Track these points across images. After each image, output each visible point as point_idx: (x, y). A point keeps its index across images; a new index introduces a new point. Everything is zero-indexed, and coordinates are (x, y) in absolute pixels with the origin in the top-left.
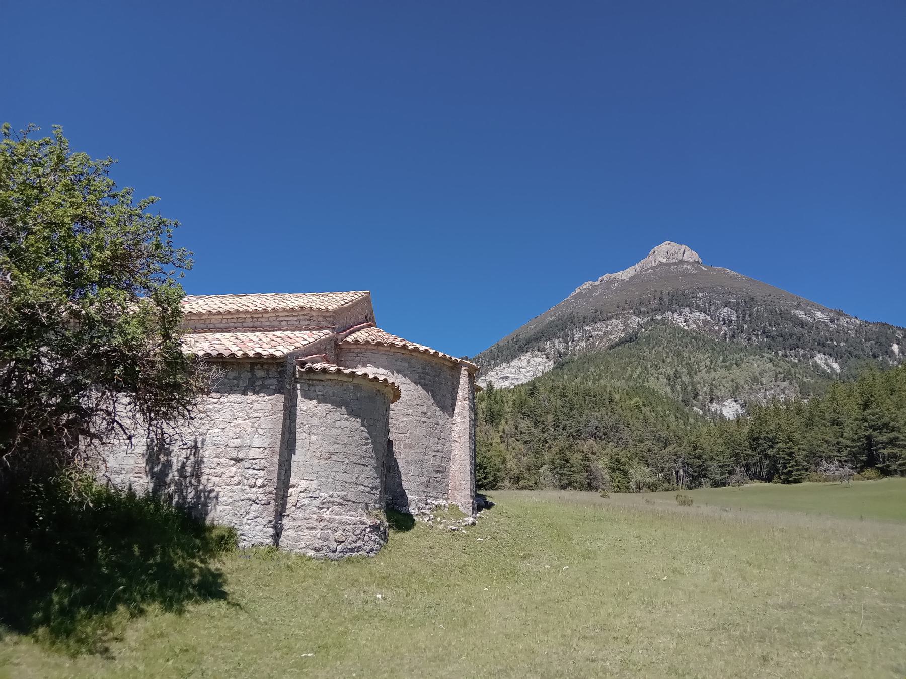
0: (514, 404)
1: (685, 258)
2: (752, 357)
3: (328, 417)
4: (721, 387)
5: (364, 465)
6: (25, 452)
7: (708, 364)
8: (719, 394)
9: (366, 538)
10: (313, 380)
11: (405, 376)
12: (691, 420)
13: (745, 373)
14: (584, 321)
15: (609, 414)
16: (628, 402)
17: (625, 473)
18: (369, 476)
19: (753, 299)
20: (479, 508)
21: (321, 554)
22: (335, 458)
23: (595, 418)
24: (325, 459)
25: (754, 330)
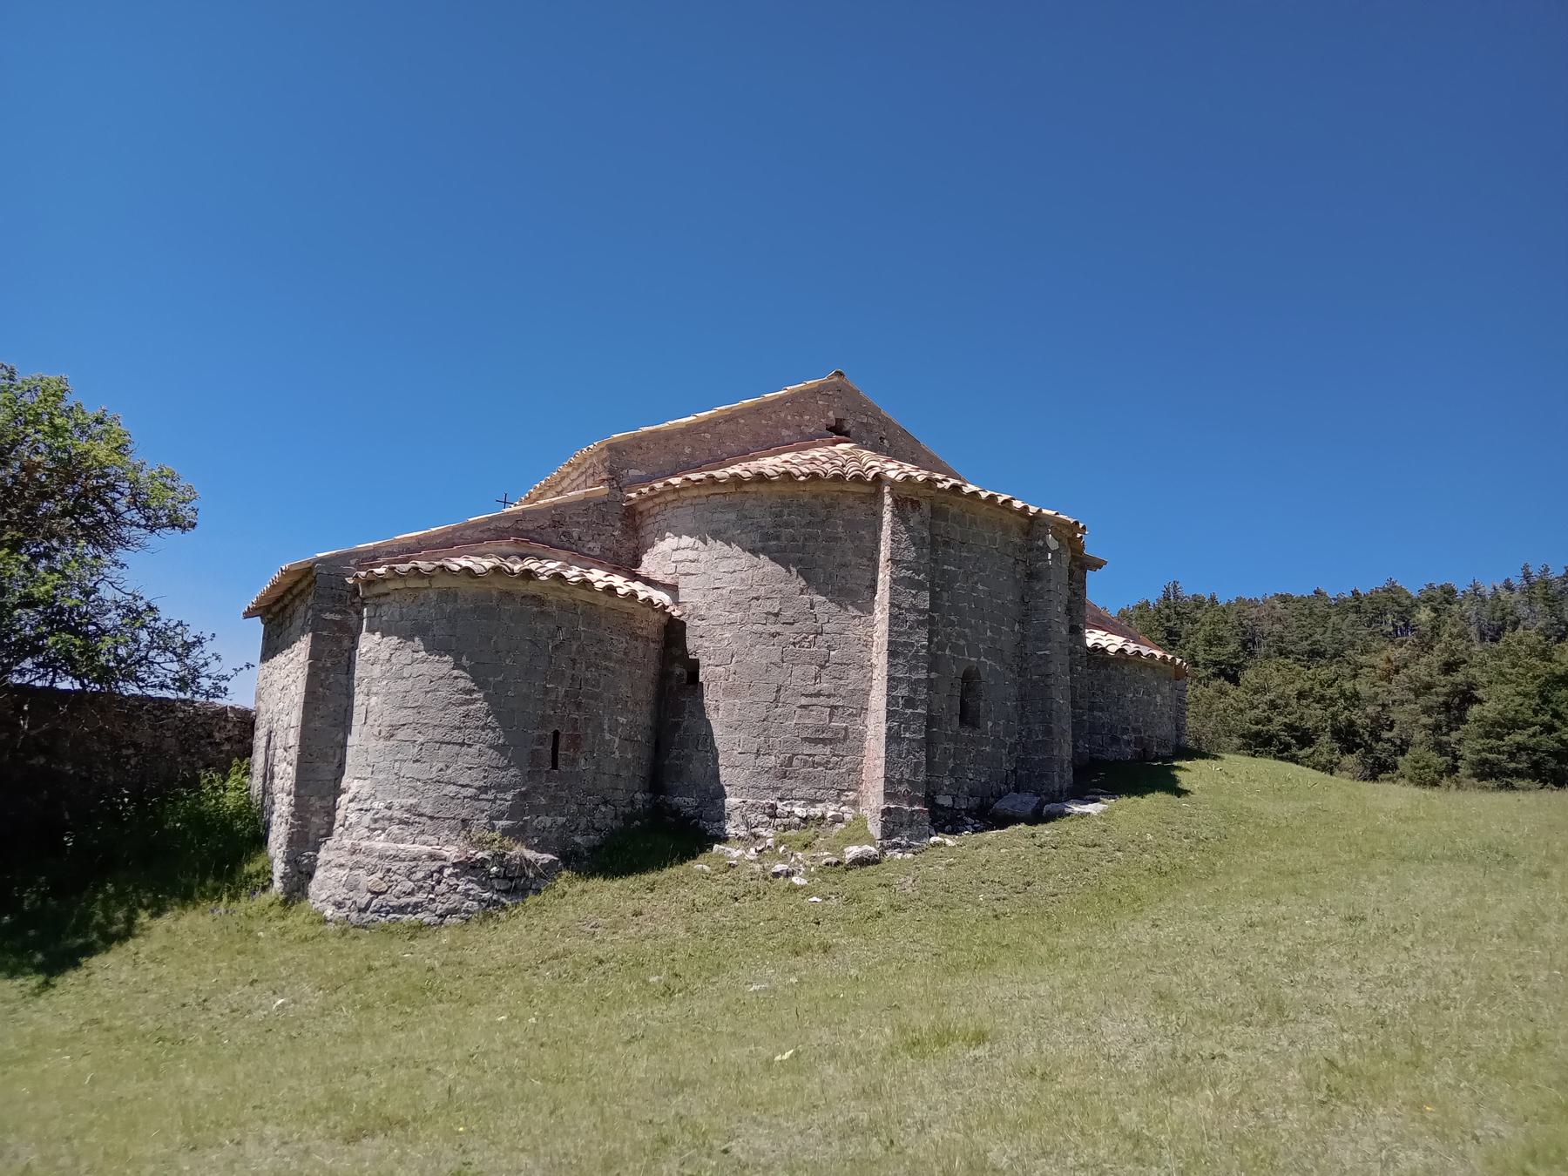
3: (394, 660)
5: (462, 744)
6: (128, 757)
9: (443, 888)
10: (378, 596)
22: (401, 735)
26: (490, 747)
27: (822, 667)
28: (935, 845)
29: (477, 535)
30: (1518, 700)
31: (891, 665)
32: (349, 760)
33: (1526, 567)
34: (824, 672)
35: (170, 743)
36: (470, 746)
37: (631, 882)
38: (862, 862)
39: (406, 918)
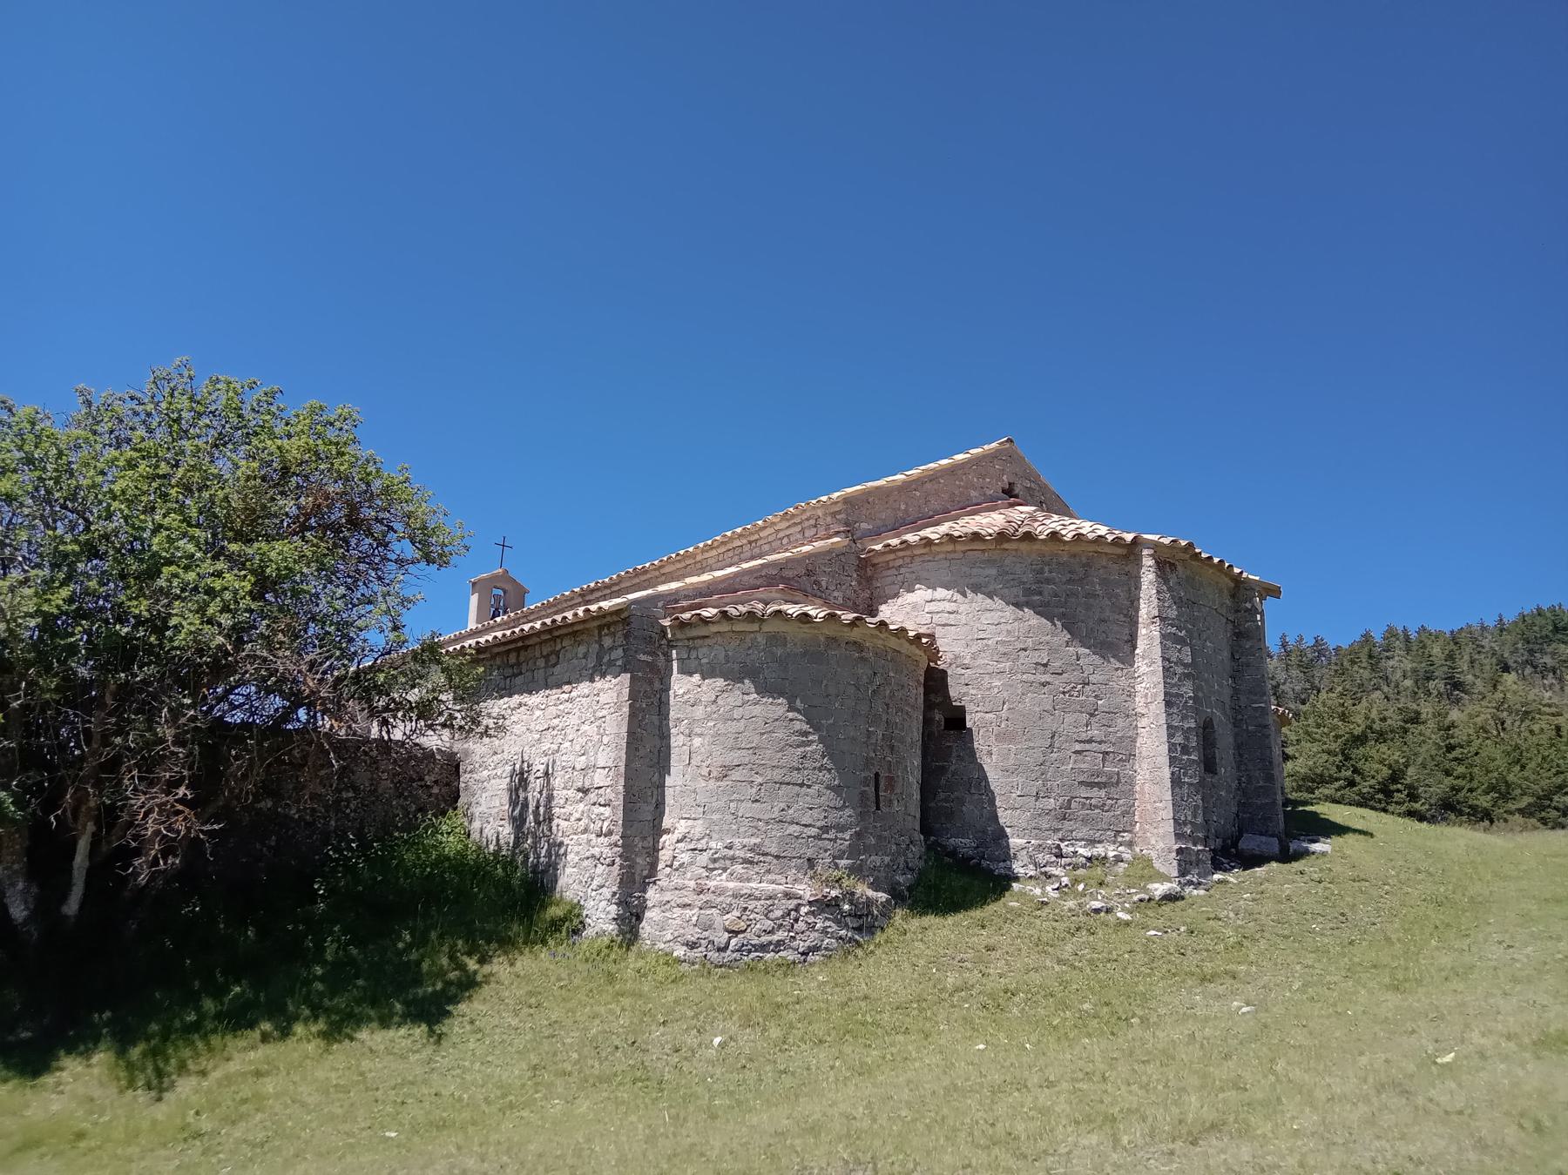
3: (720, 702)
5: (801, 785)
6: (348, 800)
9: (801, 926)
10: (693, 638)
21: (696, 954)
22: (736, 775)
24: (718, 779)
27: (1092, 715)
28: (1220, 882)
29: (753, 582)
30: (1325, 757)
31: (1168, 715)
32: (669, 800)
33: (1284, 636)
34: (1093, 720)
35: (386, 784)
36: (809, 787)
37: (962, 919)
38: (1170, 898)
39: (768, 956)
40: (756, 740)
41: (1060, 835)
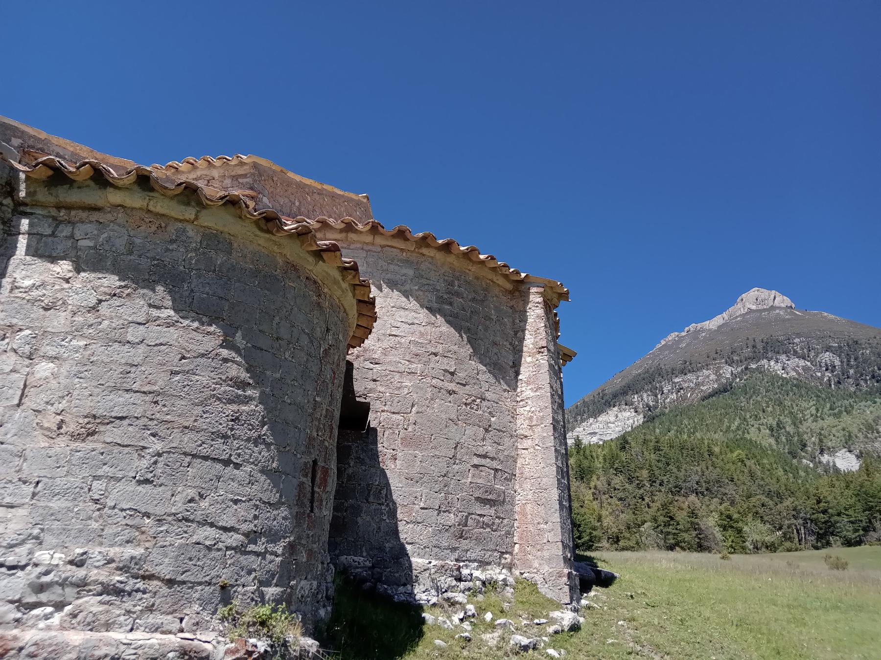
0: (605, 460)
1: (777, 303)
2: (863, 403)
3: (104, 309)
4: (832, 437)
5: (227, 463)
7: (814, 412)
8: (830, 444)
10: (69, 208)
11: (406, 294)
12: (802, 474)
13: (858, 421)
14: (673, 372)
15: (711, 468)
16: (729, 455)
17: (739, 531)
18: (241, 497)
19: (856, 342)
20: (585, 587)
22: (112, 433)
23: (694, 472)
25: (862, 375)
26: (263, 471)
27: (487, 430)
34: (488, 436)
36: (237, 466)
40: (161, 381)
41: (456, 555)
